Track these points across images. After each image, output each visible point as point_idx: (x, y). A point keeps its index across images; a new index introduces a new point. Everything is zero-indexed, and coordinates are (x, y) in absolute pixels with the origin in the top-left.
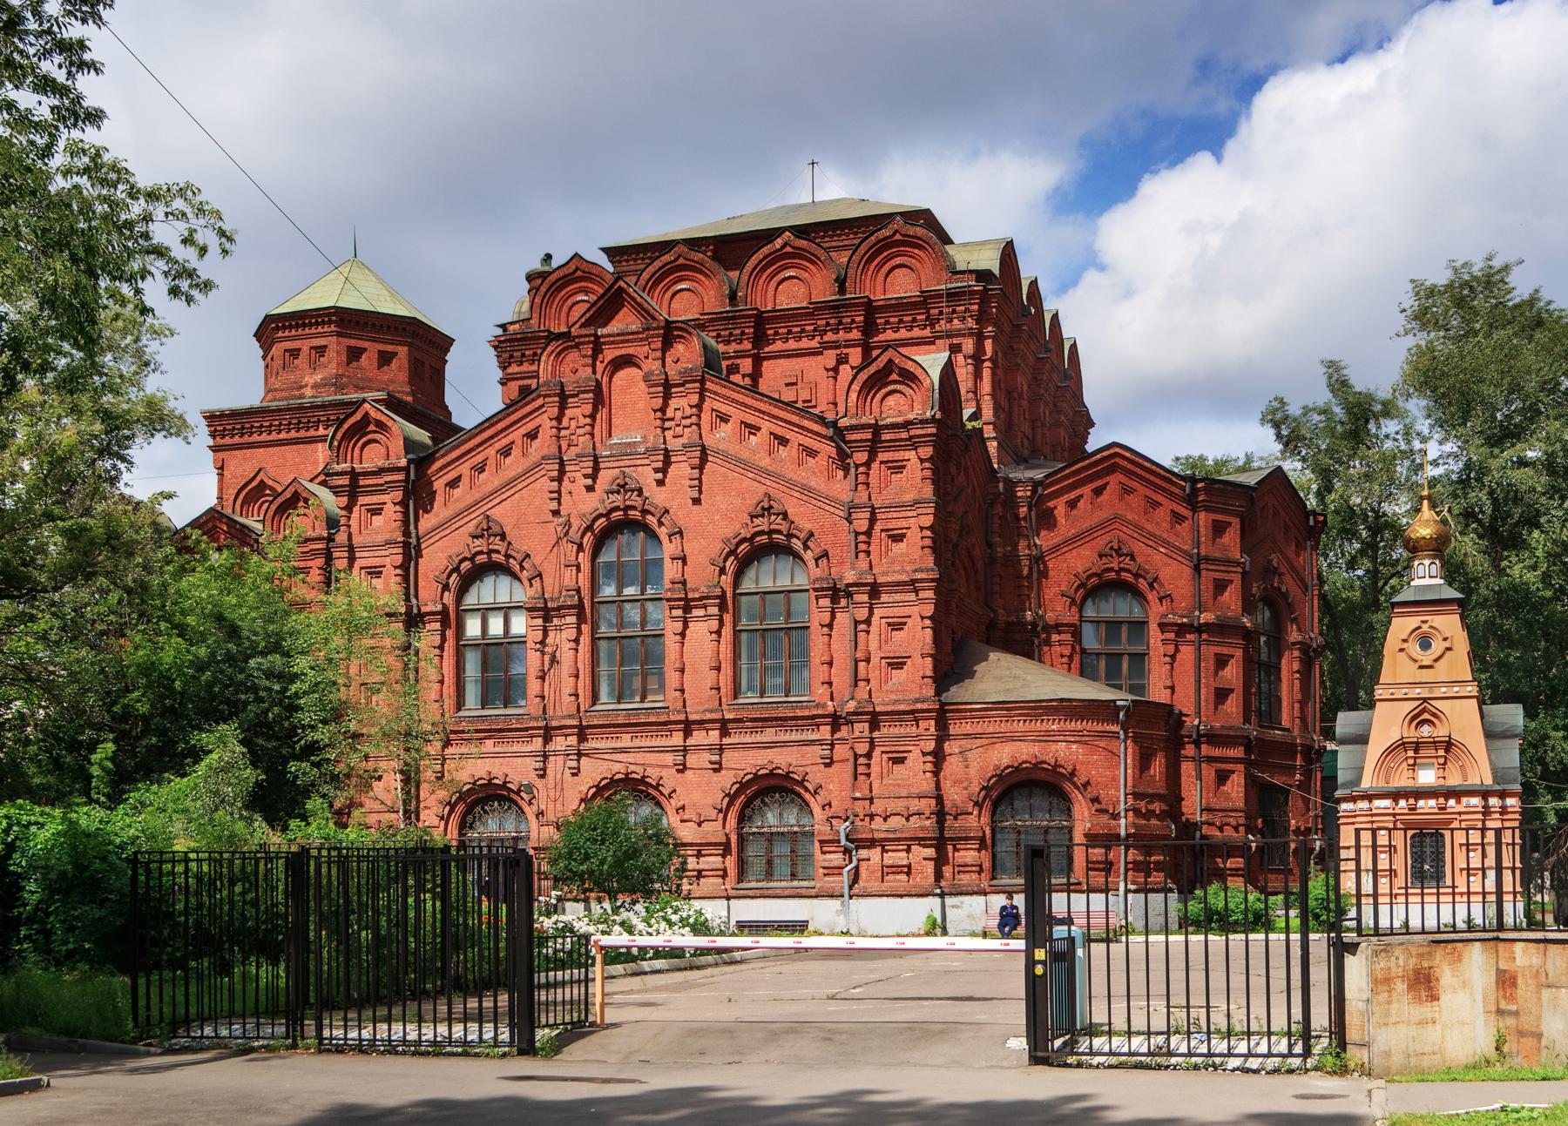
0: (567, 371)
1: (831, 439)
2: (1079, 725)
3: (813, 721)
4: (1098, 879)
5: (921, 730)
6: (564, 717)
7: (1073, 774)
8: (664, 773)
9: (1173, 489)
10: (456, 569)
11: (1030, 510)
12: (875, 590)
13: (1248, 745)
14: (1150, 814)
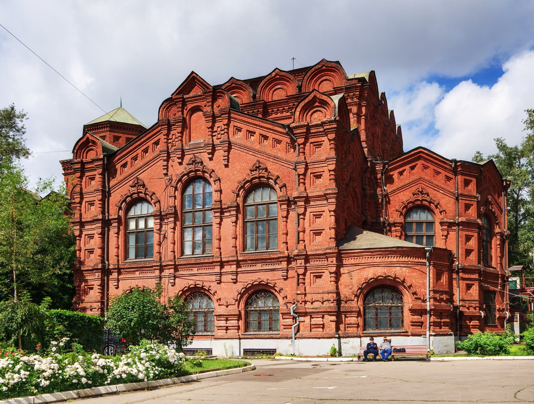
0: (172, 115)
1: (287, 134)
2: (406, 259)
3: (278, 260)
4: (418, 330)
5: (329, 263)
6: (168, 261)
7: (404, 281)
8: (212, 284)
9: (446, 166)
10: (125, 201)
11: (382, 175)
12: (307, 200)
13: (479, 272)
14: (441, 300)
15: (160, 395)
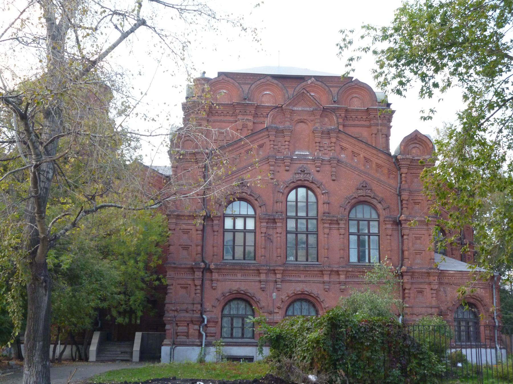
15: (100, 7)
